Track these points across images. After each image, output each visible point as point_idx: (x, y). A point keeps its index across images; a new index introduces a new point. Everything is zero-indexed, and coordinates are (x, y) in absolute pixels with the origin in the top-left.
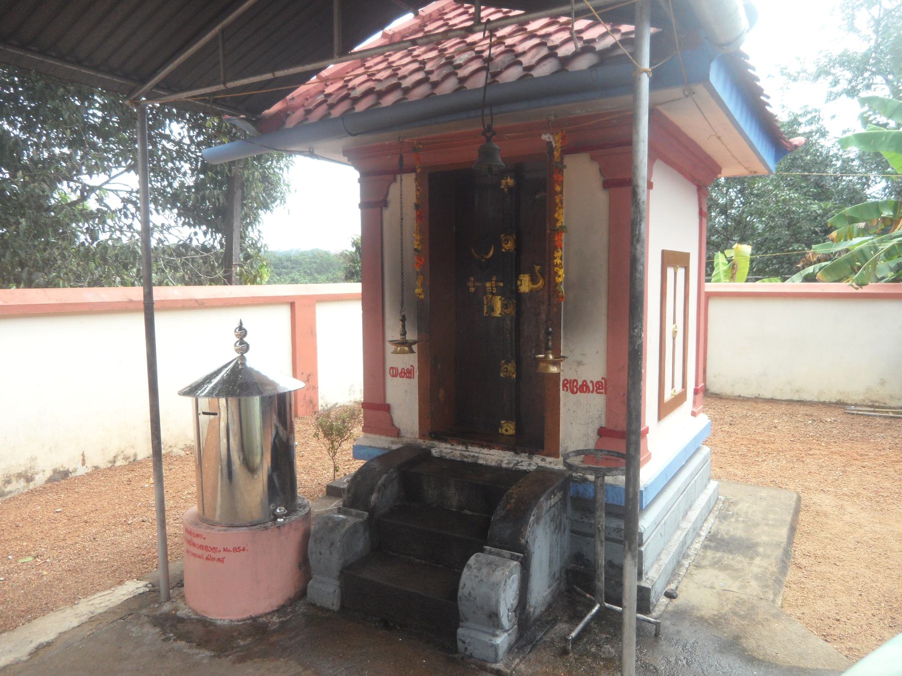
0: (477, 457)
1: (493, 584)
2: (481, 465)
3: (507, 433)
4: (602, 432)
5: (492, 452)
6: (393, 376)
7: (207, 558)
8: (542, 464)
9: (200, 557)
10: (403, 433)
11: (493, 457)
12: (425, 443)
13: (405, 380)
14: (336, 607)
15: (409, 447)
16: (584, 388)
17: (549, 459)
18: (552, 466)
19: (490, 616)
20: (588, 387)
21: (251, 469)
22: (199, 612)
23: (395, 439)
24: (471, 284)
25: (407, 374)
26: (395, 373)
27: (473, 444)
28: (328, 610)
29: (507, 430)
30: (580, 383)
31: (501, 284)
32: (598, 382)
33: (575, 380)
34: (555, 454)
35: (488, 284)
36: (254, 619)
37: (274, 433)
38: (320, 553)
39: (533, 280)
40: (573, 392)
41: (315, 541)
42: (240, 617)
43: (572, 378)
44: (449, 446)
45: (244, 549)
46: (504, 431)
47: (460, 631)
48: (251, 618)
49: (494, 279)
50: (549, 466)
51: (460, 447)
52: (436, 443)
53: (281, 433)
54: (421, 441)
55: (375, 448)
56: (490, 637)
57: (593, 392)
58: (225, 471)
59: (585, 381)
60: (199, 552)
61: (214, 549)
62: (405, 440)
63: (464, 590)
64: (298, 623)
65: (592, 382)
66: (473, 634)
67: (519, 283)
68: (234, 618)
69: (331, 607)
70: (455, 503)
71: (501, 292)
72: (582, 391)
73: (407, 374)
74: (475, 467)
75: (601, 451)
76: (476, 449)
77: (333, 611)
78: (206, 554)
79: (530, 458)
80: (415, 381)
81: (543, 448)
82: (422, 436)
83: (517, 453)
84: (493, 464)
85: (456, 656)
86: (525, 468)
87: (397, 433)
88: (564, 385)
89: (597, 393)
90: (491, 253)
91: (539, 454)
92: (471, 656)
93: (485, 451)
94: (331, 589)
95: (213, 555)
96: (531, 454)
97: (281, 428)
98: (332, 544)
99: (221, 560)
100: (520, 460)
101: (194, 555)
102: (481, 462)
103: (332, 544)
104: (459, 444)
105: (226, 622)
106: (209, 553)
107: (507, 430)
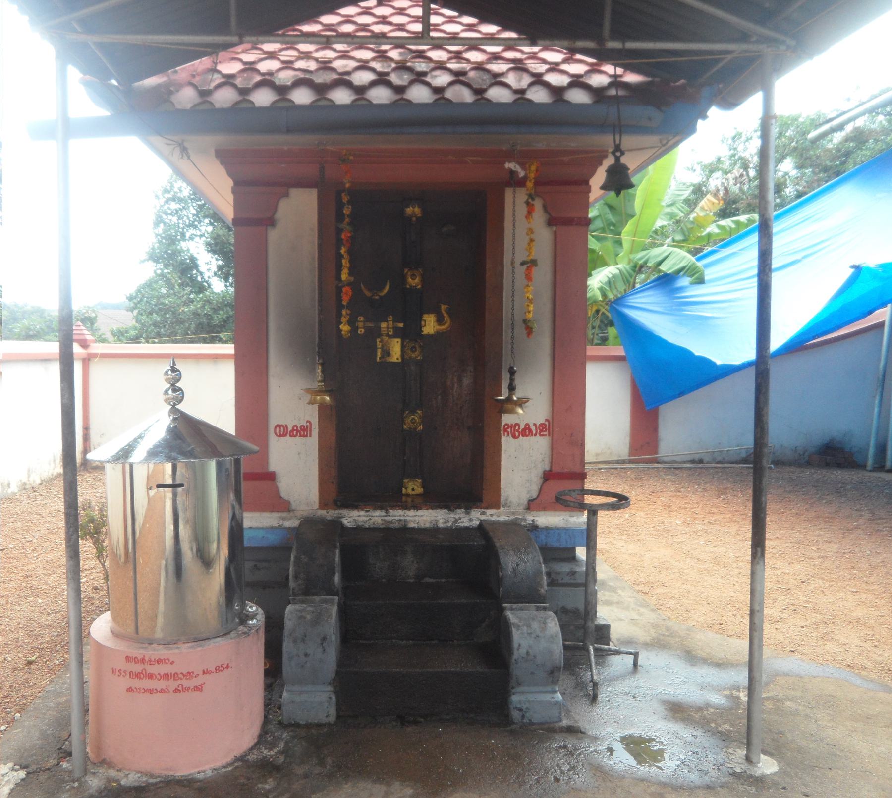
0: (405, 521)
1: (552, 637)
2: (413, 528)
3: (413, 493)
4: (548, 476)
5: (420, 512)
6: (280, 436)
7: (176, 691)
8: (483, 517)
9: (162, 691)
10: (294, 505)
11: (424, 518)
12: (330, 514)
13: (298, 439)
14: (332, 719)
15: (308, 522)
16: (527, 431)
17: (489, 512)
18: (494, 518)
19: (552, 672)
20: (530, 431)
21: (206, 562)
22: (157, 772)
23: (285, 514)
24: (361, 325)
25: (302, 431)
26: (282, 432)
27: (394, 507)
28: (319, 725)
29: (413, 490)
30: (522, 427)
31: (401, 325)
32: (541, 425)
33: (517, 424)
34: (496, 505)
35: (383, 325)
36: (241, 759)
37: (231, 515)
38: (306, 655)
39: (440, 321)
40: (514, 437)
41: (295, 642)
42: (229, 759)
43: (514, 423)
44: (362, 513)
45: (228, 667)
46: (410, 491)
47: (515, 699)
48: (237, 759)
49: (390, 318)
50: (490, 518)
51: (378, 513)
52: (345, 512)
53: (237, 512)
54: (323, 513)
55: (258, 528)
56: (551, 696)
57: (535, 435)
58: (171, 568)
59: (527, 424)
60: (162, 684)
61: (189, 675)
62: (299, 514)
63: (521, 651)
64: (288, 749)
65: (535, 424)
66: (531, 697)
67: (423, 323)
68: (218, 764)
69: (324, 720)
70: (411, 573)
71: (397, 333)
72: (524, 435)
73: (302, 431)
74: (404, 529)
75: (574, 491)
76: (401, 512)
77: (329, 724)
78: (173, 684)
79: (468, 513)
80: (313, 441)
81: (481, 500)
82: (323, 505)
83: (450, 509)
84: (428, 525)
85: (514, 727)
86: (467, 524)
87: (282, 505)
88: (505, 430)
89: (541, 435)
90: (387, 288)
91: (477, 507)
92: (531, 723)
93: (411, 513)
94: (324, 697)
95: (186, 683)
96: (468, 509)
97: (237, 507)
98: (324, 639)
99: (198, 688)
100: (457, 516)
101: (151, 691)
102: (411, 525)
103: (324, 639)
104: (375, 509)
105: (209, 773)
106: (180, 682)
107: (413, 490)
